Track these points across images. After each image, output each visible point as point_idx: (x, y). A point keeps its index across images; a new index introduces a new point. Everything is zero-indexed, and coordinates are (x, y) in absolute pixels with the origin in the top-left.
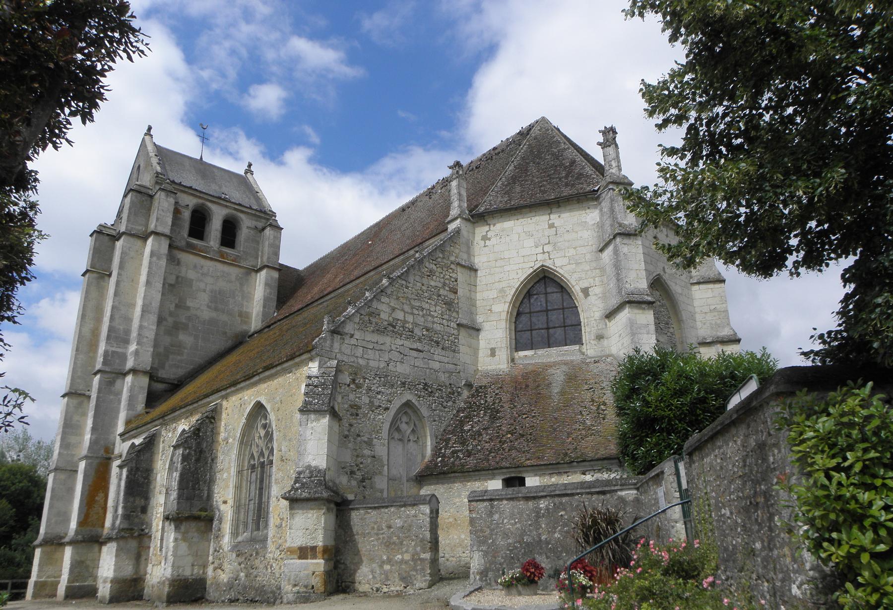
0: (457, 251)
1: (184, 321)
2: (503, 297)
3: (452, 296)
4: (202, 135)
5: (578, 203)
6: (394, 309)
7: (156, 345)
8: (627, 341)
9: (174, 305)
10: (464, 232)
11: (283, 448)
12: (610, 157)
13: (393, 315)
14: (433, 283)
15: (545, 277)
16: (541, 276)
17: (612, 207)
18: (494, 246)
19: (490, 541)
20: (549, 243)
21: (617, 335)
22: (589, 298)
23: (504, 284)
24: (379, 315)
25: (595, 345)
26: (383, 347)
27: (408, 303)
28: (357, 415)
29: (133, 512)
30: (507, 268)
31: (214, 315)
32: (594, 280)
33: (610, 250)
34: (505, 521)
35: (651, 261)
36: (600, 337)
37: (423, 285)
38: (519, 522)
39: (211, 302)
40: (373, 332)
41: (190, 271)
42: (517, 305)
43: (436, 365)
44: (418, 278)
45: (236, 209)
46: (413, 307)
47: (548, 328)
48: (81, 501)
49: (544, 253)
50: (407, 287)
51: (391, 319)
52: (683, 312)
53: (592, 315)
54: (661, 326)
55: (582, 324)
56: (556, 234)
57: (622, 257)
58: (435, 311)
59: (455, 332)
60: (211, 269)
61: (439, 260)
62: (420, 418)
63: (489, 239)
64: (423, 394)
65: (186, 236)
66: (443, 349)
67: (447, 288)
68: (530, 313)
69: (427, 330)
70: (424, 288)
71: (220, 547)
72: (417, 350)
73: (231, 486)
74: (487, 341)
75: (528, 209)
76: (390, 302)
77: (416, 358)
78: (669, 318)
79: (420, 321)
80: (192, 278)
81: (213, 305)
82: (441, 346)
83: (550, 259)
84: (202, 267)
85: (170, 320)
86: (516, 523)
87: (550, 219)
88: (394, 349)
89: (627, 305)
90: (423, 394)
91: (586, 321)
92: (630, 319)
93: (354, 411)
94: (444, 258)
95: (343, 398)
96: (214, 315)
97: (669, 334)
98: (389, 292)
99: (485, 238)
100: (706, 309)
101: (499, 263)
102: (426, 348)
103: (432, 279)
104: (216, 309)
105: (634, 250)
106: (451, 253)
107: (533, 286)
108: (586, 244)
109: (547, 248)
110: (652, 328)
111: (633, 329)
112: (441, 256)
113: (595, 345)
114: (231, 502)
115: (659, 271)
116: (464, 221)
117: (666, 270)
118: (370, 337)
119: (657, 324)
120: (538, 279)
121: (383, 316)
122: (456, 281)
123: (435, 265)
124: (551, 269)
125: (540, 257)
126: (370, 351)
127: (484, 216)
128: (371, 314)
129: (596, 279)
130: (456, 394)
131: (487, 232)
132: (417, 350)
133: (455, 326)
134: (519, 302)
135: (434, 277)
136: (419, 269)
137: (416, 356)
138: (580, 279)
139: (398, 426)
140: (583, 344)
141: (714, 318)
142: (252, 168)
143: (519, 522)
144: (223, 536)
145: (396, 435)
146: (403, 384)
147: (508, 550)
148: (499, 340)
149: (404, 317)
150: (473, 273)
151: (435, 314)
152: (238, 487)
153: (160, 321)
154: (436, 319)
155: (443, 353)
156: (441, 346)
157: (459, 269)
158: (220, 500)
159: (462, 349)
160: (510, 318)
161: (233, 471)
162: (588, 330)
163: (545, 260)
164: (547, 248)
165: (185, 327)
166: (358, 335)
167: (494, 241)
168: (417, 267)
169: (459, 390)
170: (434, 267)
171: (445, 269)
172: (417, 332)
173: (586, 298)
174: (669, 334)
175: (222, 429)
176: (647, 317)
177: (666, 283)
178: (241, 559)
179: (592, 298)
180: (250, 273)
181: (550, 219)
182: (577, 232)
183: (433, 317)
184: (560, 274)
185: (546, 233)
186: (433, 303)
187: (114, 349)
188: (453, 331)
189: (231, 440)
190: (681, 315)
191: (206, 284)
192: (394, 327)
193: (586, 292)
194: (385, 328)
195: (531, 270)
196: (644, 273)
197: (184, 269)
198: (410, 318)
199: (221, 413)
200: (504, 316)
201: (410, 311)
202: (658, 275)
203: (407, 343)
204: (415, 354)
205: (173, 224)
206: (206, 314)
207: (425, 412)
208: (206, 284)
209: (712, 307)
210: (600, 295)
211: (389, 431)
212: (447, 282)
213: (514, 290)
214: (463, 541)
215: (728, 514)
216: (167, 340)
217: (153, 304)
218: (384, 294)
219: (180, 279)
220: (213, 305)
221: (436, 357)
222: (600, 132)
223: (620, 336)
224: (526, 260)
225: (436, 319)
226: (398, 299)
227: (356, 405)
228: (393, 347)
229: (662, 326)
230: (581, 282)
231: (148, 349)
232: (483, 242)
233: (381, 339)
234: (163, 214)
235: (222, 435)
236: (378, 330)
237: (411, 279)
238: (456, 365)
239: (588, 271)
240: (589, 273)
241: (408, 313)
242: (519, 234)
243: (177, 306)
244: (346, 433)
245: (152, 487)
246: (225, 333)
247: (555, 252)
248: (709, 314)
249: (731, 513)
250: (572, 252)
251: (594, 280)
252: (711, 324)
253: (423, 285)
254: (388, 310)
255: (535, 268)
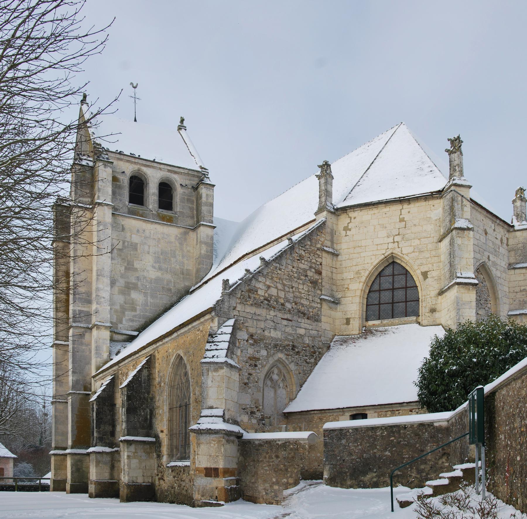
0: (322, 239)
1: (134, 281)
2: (358, 278)
3: (317, 277)
4: (133, 96)
5: (425, 201)
6: (269, 287)
7: (112, 303)
8: (453, 314)
9: (123, 268)
10: (329, 224)
11: (196, 392)
12: (456, 163)
13: (269, 292)
14: (302, 266)
15: (394, 262)
16: (391, 261)
17: (452, 205)
18: (353, 235)
19: (338, 458)
20: (399, 235)
21: (446, 310)
22: (427, 279)
23: (359, 268)
24: (257, 291)
25: (429, 316)
26: (259, 318)
27: (281, 282)
28: (256, 366)
29: (105, 435)
30: (363, 255)
31: (159, 274)
32: (433, 265)
33: (447, 241)
34: (350, 444)
35: (479, 251)
36: (433, 311)
37: (293, 267)
38: (361, 445)
39: (155, 262)
40: (252, 305)
41: (133, 236)
42: (370, 284)
43: (302, 331)
44: (289, 262)
45: (169, 171)
46: (284, 285)
47: (406, 302)
48: (72, 426)
49: (394, 242)
50: (280, 269)
51: (267, 295)
52: (499, 292)
53: (428, 293)
54: (480, 303)
55: (420, 300)
56: (405, 227)
57: (456, 248)
58: (303, 289)
59: (319, 306)
60: (152, 232)
61: (307, 247)
62: (289, 371)
63: (350, 230)
64: (291, 353)
65: (127, 203)
66: (308, 318)
67: (313, 270)
68: (380, 291)
69: (296, 304)
70: (294, 270)
71: (161, 464)
72: (287, 320)
73: (165, 420)
74: (344, 313)
75: (384, 205)
76: (266, 282)
77: (286, 326)
78: (488, 296)
79: (290, 296)
80: (137, 242)
81: (157, 265)
82: (306, 316)
83: (399, 247)
84: (144, 231)
85: (121, 282)
86: (358, 445)
87: (401, 214)
88: (269, 319)
89: (457, 286)
90: (291, 353)
91: (423, 298)
92: (457, 297)
93: (253, 362)
94: (311, 245)
95: (242, 352)
96: (159, 274)
97: (487, 308)
98: (265, 272)
99: (346, 229)
100: (517, 289)
101: (358, 250)
102: (295, 318)
103: (301, 263)
104: (160, 269)
105: (466, 243)
106: (317, 241)
107: (383, 270)
108: (429, 236)
109: (397, 239)
110: (474, 304)
111: (458, 305)
112: (309, 243)
113: (429, 316)
114: (166, 431)
115: (485, 259)
116: (330, 214)
117: (490, 258)
118: (249, 309)
119: (478, 301)
120: (388, 263)
121: (260, 292)
122: (321, 264)
123: (304, 251)
124: (399, 255)
125: (391, 246)
126: (249, 320)
127: (346, 210)
128: (250, 291)
129: (434, 265)
130: (317, 353)
131: (349, 223)
132: (287, 320)
133: (319, 301)
134: (371, 282)
135: (303, 261)
136: (291, 254)
137: (286, 324)
138: (421, 264)
139: (271, 377)
140: (419, 316)
141: (523, 296)
142: (185, 123)
143: (361, 445)
144: (163, 456)
145: (269, 383)
146: (276, 346)
147: (351, 463)
148: (353, 312)
149: (278, 293)
150: (335, 258)
151: (303, 292)
152: (170, 420)
153: (113, 283)
154: (303, 295)
155: (309, 322)
156: (306, 316)
157: (325, 255)
158: (159, 430)
159: (323, 319)
160: (363, 295)
161: (166, 408)
162: (424, 305)
163: (394, 248)
164: (397, 239)
165: (135, 287)
166: (239, 307)
167: (353, 231)
168: (289, 252)
169: (320, 350)
170: (303, 253)
171: (312, 255)
172: (288, 306)
173: (425, 279)
174: (487, 308)
175: (157, 376)
176: (471, 296)
177: (489, 269)
178: (174, 474)
179: (429, 280)
180: (188, 233)
181: (401, 214)
182: (422, 226)
183: (300, 293)
184: (406, 260)
185: (397, 226)
186: (301, 282)
187: (79, 308)
188: (315, 305)
189: (162, 384)
190: (498, 294)
191: (149, 246)
192: (269, 301)
193: (425, 275)
194: (262, 302)
195: (383, 257)
196: (472, 261)
197: (128, 234)
198: (282, 294)
199: (155, 363)
200: (358, 293)
201: (282, 289)
202: (484, 262)
203: (280, 315)
204: (285, 322)
205: (114, 193)
206: (153, 274)
207: (292, 367)
208: (149, 246)
209: (522, 288)
210: (436, 278)
211: (264, 381)
212: (314, 266)
213: (368, 272)
214: (319, 457)
215: (503, 439)
216: (120, 299)
217: (105, 269)
218: (261, 274)
219: (126, 244)
220: (157, 265)
221: (302, 325)
222: (449, 140)
223: (448, 310)
224: (379, 247)
225: (303, 295)
226: (272, 279)
227: (255, 358)
228: (268, 317)
229: (482, 302)
230: (422, 267)
231: (106, 308)
232: (345, 232)
233: (259, 311)
234: (104, 184)
235: (157, 380)
236: (256, 304)
237: (284, 262)
238: (318, 331)
239: (428, 258)
240: (429, 259)
241: (281, 290)
242: (375, 226)
243: (126, 268)
244: (246, 381)
245: (116, 417)
246: (170, 290)
247: (403, 242)
248: (518, 294)
249: (505, 438)
250: (417, 242)
251: (433, 265)
252: (520, 301)
253: (293, 267)
254: (264, 288)
255: (386, 255)
